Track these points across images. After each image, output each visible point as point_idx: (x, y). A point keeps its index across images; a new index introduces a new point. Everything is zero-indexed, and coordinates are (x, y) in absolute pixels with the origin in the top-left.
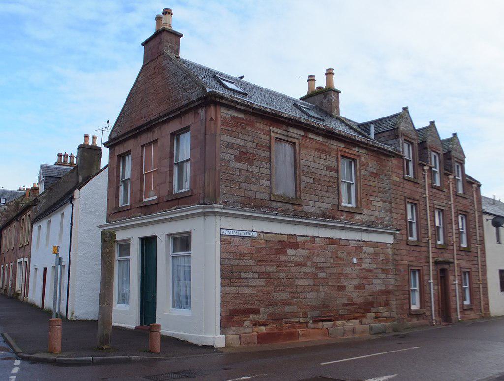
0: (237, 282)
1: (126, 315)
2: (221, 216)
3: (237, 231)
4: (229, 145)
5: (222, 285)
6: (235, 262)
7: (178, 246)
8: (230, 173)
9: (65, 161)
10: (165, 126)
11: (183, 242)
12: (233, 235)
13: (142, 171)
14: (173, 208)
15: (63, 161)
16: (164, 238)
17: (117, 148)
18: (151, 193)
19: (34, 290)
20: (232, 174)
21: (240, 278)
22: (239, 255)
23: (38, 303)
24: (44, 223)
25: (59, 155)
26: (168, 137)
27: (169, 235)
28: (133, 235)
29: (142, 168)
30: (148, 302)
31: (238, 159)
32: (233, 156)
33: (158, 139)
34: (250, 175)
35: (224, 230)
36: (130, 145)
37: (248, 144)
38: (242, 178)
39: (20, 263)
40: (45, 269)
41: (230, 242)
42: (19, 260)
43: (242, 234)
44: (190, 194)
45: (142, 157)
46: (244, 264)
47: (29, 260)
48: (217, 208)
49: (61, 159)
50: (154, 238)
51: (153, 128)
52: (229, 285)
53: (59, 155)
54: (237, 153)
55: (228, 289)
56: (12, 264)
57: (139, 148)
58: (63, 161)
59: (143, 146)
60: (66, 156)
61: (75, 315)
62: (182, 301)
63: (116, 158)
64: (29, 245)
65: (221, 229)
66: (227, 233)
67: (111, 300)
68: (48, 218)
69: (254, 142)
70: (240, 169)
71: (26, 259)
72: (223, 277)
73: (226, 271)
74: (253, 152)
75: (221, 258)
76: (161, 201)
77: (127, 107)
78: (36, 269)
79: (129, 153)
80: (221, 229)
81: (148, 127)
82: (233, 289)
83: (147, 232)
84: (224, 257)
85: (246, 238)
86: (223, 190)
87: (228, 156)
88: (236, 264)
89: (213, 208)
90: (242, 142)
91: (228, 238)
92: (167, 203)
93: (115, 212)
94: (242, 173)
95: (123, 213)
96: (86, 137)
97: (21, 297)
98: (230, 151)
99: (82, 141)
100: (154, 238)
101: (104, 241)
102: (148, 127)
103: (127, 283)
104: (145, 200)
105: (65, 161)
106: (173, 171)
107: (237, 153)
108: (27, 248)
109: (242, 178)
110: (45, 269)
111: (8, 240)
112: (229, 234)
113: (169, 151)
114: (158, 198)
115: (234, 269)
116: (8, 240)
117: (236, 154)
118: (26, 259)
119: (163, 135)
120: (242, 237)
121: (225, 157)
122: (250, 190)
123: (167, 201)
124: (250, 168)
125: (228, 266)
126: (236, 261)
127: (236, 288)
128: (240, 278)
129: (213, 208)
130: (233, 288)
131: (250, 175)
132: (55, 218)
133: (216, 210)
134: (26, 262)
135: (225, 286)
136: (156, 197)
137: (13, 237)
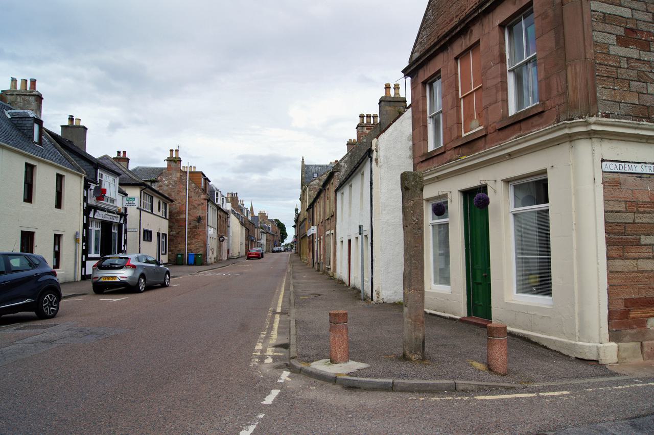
0: (633, 252)
1: (447, 294)
2: (602, 139)
3: (630, 164)
4: (606, 18)
5: (608, 258)
6: (629, 218)
7: (520, 202)
8: (610, 66)
9: (369, 123)
10: (486, 21)
11: (536, 189)
12: (623, 171)
13: (457, 94)
14: (511, 138)
15: (365, 122)
16: (500, 186)
17: (421, 73)
18: (475, 123)
19: (341, 263)
20: (613, 66)
21: (638, 244)
22: (634, 206)
23: (345, 277)
24: (346, 190)
25: (362, 116)
26: (496, 32)
27: (507, 182)
28: (451, 191)
29: (457, 90)
30: (478, 284)
31: (622, 41)
32: (614, 37)
33: (479, 40)
34: (646, 68)
35: (608, 163)
36: (438, 63)
37: (637, 15)
38: (633, 74)
39: (328, 235)
40: (350, 241)
41: (620, 183)
42: (327, 233)
43: (639, 169)
44: (540, 110)
45: (456, 74)
46: (645, 220)
47: (335, 232)
48: (596, 123)
49: (363, 120)
50: (484, 188)
51: (470, 27)
52: (621, 258)
53: (362, 116)
54: (620, 31)
55: (619, 264)
56: (322, 237)
57: (452, 62)
58: (365, 122)
59: (456, 59)
60: (368, 116)
61: (381, 297)
62: (540, 280)
63: (420, 86)
64: (334, 215)
65: (603, 160)
66: (612, 167)
67: (421, 281)
68: (348, 183)
69: (647, 11)
70: (628, 58)
71: (332, 231)
72: (609, 243)
73: (614, 234)
74: (646, 29)
75: (605, 212)
76: (491, 130)
77: (430, 13)
78: (342, 242)
79: (437, 75)
80: (603, 160)
81: (464, 27)
82: (628, 265)
83: (471, 181)
84: (609, 209)
85: (645, 176)
86: (603, 94)
87: (607, 37)
88: (632, 222)
89: (587, 124)
90: (627, 13)
91: (616, 176)
92: (500, 133)
93: (423, 158)
94: (633, 65)
95: (435, 159)
96: (387, 87)
97: (330, 272)
98: (609, 28)
99: (382, 93)
100: (484, 188)
101: (405, 189)
102: (464, 27)
103: (205, 210)
104: (464, 135)
105: (369, 123)
106: (506, 82)
107: (620, 31)
108: (333, 219)
109: (633, 74)
110: (350, 241)
111: (318, 213)
112: (616, 170)
113: (498, 54)
114: (486, 128)
115: (629, 229)
116: (318, 213)
117: (619, 33)
118: (332, 231)
119: (486, 31)
120: (639, 175)
121: (599, 37)
122: (647, 94)
123: (500, 130)
124: (645, 56)
125: (618, 224)
126: (631, 215)
127: (634, 262)
128: (638, 244)
129: (587, 124)
130: (628, 262)
131: (646, 68)
132: (356, 183)
133: (594, 127)
134: (332, 234)
135: (614, 258)
136: (482, 127)
137: (322, 209)
